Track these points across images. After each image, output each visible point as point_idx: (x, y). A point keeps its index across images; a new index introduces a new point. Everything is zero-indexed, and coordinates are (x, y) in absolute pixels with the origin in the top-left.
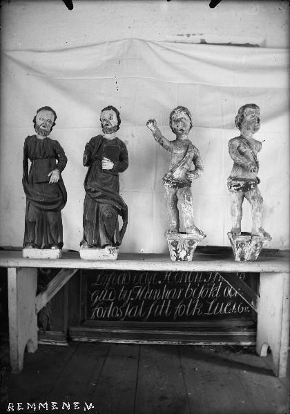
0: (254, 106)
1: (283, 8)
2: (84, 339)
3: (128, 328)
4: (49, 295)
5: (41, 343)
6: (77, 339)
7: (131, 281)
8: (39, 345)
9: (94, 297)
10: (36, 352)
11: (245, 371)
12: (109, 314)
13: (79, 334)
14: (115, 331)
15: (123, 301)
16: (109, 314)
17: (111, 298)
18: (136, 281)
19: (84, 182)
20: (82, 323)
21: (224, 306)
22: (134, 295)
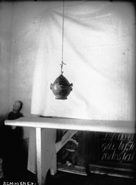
0: (56, 99)
1: (128, 7)
2: (97, 172)
3: (108, 166)
4: (63, 143)
5: (59, 170)
6: (92, 172)
7: (127, 139)
8: (58, 171)
9: (104, 147)
10: (55, 174)
11: (2, 161)
12: (112, 158)
13: (94, 169)
14: (116, 169)
15: (121, 151)
16: (112, 158)
17: (114, 148)
18: (130, 139)
19: (22, 109)
20: (95, 163)
21: (108, 159)
22: (128, 147)
